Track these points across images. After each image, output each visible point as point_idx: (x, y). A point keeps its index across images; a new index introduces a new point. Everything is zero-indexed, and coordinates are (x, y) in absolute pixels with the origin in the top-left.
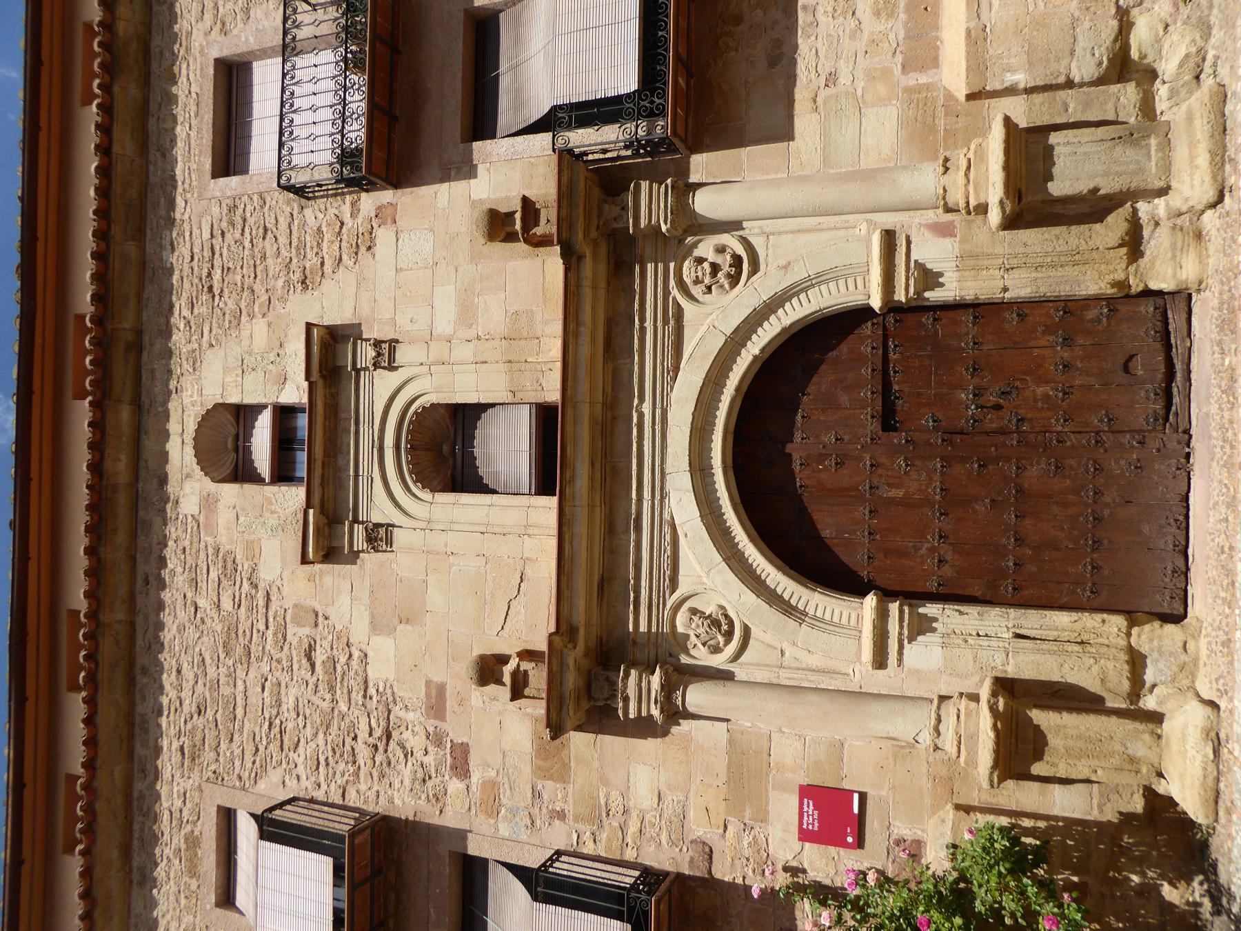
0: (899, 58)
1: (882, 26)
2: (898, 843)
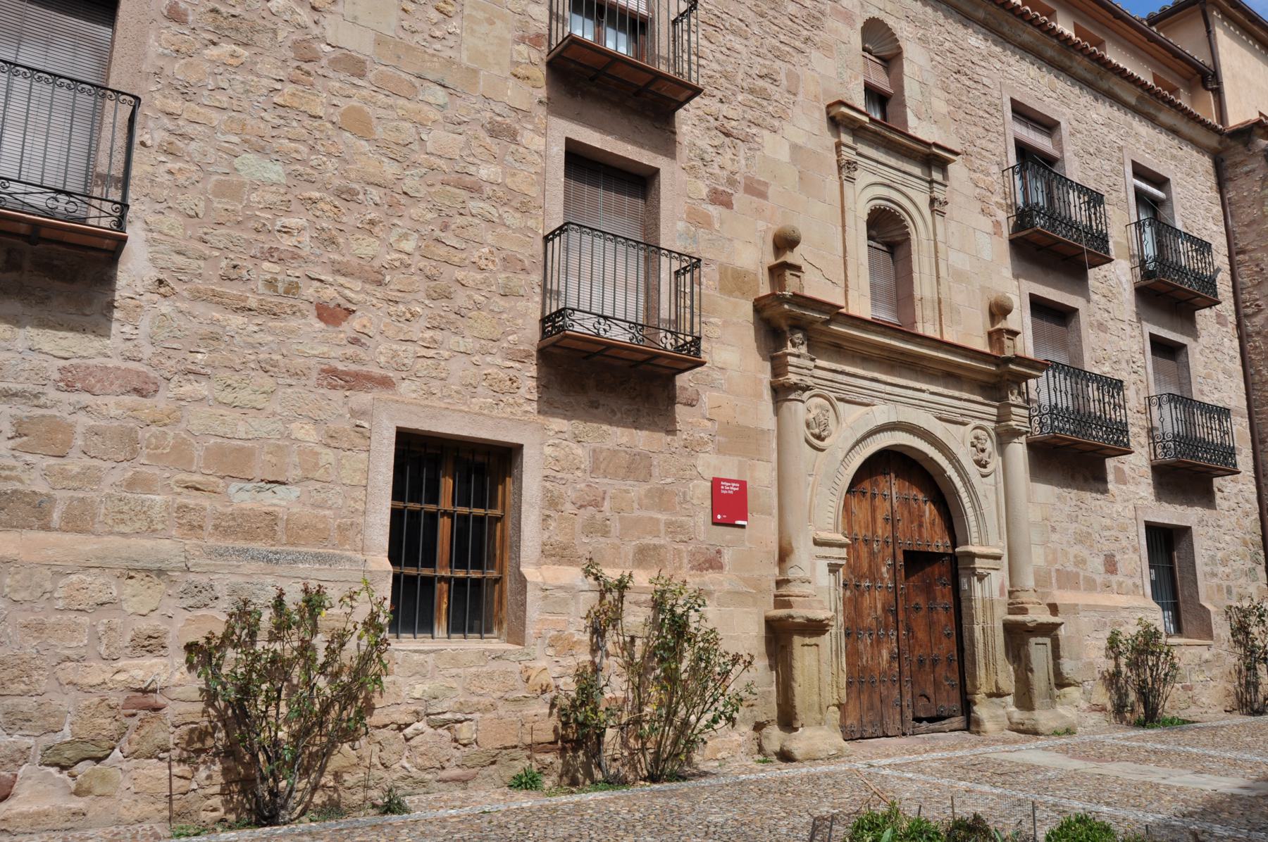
2: (719, 552)
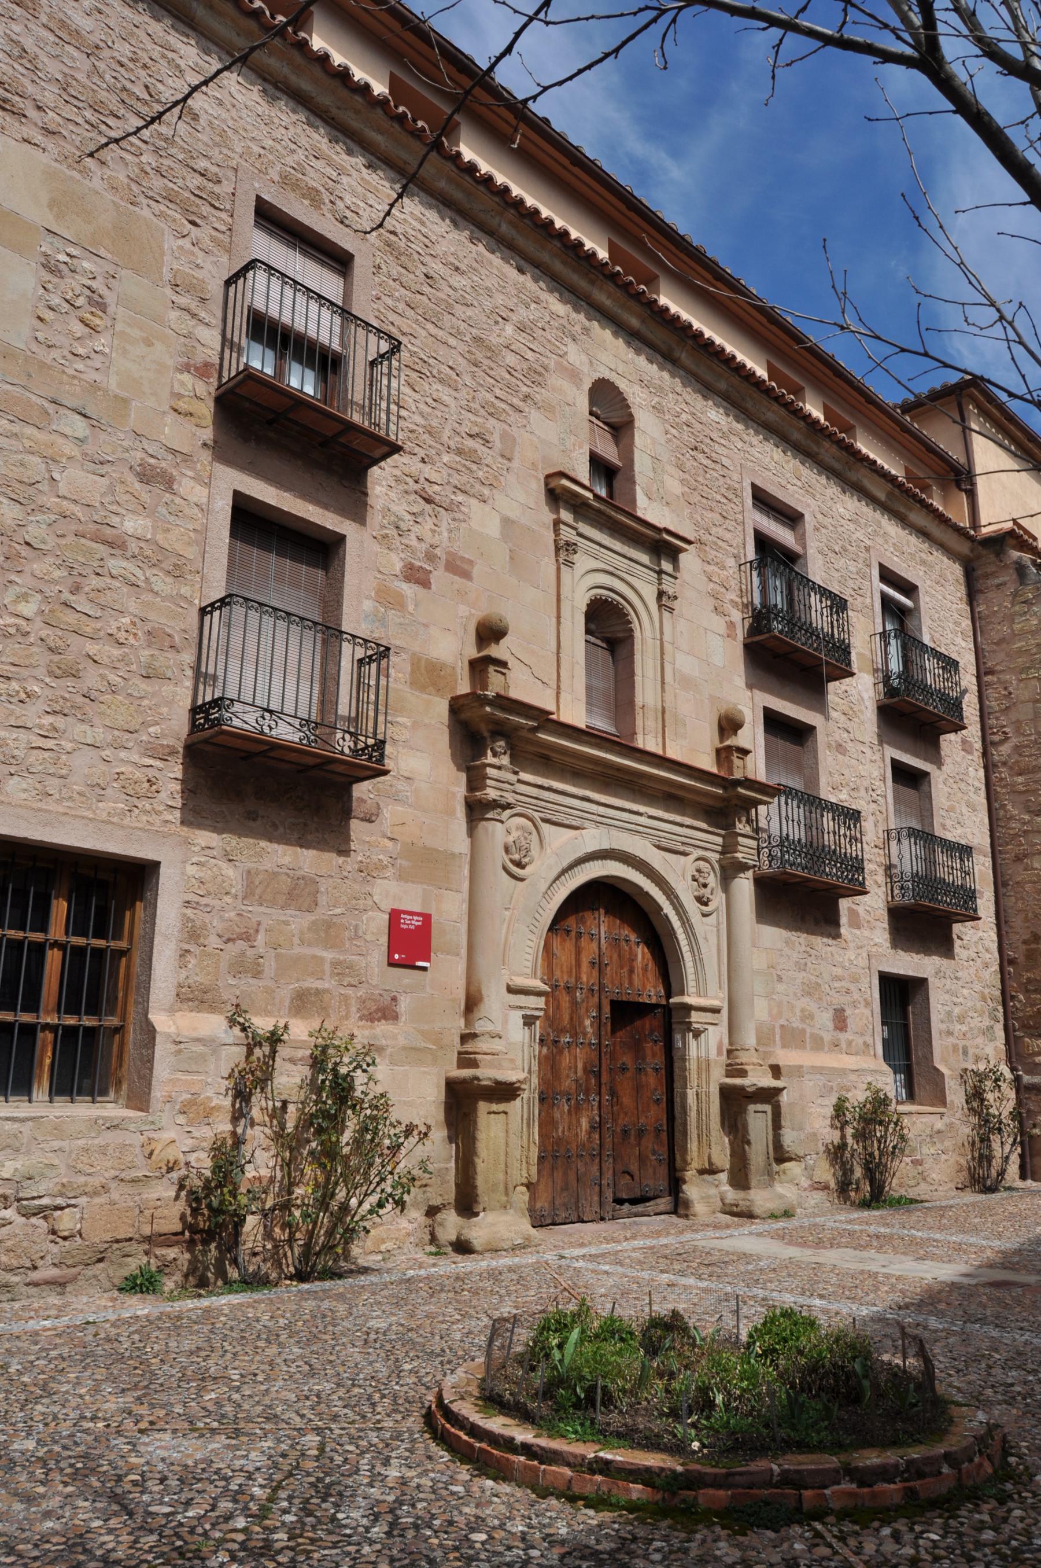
2: (394, 999)
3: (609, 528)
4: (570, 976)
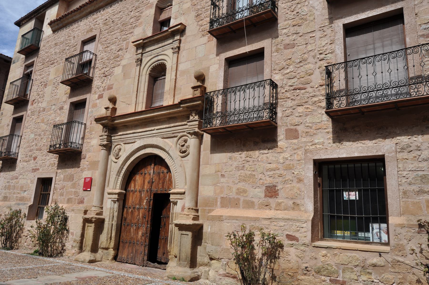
0: (225, 196)
1: (234, 190)
3: (157, 42)
4: (141, 187)
